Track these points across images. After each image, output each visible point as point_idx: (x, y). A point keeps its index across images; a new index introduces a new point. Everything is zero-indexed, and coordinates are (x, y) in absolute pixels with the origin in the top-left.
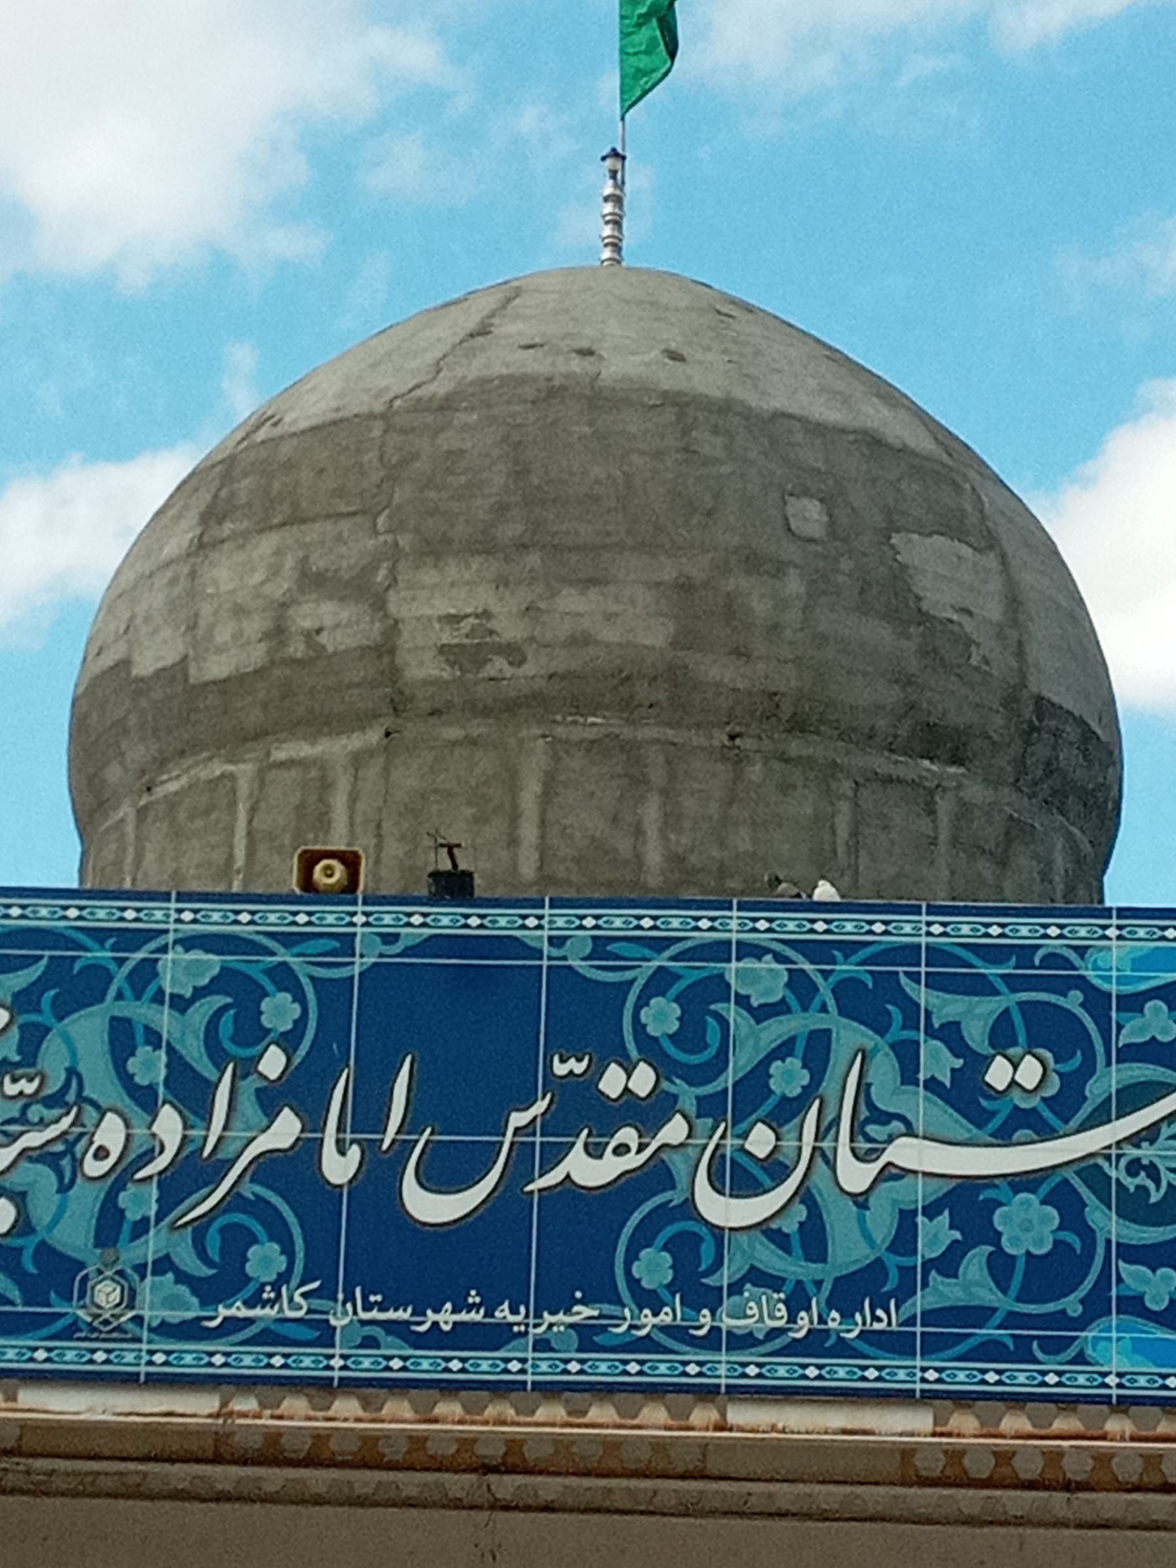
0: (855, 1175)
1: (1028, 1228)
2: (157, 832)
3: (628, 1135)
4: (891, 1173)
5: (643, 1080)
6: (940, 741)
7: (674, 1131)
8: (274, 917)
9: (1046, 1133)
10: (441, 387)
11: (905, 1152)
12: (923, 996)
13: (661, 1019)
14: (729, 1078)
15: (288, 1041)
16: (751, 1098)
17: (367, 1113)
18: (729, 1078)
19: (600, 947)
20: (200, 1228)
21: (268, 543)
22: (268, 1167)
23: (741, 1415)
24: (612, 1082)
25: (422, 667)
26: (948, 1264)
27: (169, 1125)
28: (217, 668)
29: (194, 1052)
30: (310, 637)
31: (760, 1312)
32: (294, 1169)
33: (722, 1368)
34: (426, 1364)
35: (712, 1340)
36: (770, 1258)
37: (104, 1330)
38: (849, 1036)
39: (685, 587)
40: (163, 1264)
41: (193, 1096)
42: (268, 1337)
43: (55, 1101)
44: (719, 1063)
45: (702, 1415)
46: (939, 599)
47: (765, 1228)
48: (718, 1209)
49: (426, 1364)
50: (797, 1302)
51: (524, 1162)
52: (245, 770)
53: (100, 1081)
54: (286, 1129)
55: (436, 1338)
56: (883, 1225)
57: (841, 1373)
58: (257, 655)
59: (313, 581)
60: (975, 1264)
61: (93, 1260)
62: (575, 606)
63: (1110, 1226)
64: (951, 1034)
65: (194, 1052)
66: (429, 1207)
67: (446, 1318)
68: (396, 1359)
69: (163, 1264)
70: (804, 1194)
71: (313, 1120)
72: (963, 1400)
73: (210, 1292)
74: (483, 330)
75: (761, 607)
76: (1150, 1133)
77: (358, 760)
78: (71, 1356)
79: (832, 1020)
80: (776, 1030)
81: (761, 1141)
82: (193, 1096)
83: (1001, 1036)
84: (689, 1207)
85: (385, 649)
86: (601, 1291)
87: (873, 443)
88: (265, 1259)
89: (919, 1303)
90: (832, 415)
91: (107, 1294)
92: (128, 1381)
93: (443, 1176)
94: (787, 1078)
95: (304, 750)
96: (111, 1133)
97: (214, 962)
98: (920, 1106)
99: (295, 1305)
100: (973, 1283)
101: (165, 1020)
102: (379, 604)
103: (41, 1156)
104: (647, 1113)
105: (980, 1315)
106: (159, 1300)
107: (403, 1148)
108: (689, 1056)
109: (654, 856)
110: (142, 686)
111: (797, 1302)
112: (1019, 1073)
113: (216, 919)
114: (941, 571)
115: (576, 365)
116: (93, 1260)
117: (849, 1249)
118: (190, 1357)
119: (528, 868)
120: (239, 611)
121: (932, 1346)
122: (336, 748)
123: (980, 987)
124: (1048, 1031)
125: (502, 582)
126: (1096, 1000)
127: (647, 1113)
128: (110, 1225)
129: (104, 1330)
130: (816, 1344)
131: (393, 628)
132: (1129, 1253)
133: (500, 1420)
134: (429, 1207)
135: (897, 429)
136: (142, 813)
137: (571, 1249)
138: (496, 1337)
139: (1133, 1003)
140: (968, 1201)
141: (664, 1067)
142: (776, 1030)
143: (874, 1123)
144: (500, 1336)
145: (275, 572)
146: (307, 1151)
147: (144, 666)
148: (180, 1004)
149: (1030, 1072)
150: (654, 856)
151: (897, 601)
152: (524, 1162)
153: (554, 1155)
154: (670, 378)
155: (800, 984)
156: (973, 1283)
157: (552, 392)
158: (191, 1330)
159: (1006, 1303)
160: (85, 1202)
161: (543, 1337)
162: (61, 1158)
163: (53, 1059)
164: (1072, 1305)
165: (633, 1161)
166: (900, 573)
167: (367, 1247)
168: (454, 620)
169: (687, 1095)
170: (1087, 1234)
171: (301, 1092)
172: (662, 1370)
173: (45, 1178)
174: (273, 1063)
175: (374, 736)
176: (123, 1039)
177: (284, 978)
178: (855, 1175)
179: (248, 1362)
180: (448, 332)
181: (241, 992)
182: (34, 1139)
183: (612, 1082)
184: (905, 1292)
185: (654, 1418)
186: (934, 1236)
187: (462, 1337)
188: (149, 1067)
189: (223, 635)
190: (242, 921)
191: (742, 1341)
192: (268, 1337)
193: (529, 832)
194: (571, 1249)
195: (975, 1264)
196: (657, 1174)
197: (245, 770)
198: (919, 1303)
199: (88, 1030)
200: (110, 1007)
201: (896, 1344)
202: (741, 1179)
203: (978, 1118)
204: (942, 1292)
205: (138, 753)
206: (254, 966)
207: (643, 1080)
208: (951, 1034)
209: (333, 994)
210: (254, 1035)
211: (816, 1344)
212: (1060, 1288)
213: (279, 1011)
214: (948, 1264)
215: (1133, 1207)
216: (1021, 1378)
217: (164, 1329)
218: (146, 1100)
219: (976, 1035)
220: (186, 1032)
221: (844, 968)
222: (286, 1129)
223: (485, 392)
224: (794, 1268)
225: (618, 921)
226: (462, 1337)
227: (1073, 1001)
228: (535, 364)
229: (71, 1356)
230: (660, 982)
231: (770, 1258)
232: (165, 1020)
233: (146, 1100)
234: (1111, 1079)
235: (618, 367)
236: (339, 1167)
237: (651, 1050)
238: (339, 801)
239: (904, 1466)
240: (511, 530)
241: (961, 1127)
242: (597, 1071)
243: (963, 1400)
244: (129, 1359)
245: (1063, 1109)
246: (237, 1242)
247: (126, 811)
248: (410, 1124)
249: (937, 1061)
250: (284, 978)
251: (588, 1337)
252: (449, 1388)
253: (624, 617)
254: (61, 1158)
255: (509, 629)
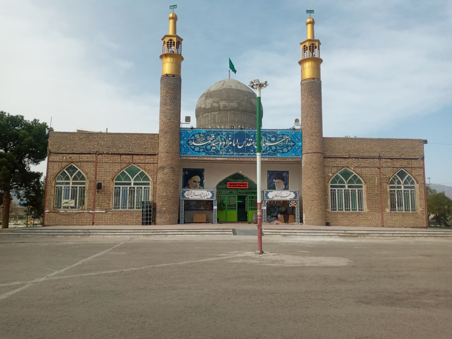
0: (264, 145)
1: (274, 148)
2: (203, 119)
5: (251, 140)
7: (253, 143)
8: (229, 130)
10: (221, 89)
11: (266, 144)
13: (252, 136)
17: (235, 142)
24: (250, 140)
25: (222, 108)
26: (269, 150)
27: (224, 143)
28: (207, 107)
29: (225, 138)
39: (238, 103)
41: (225, 141)
46: (254, 103)
49: (239, 156)
51: (245, 145)
52: (210, 114)
53: (220, 140)
54: (231, 143)
55: (240, 155)
56: (265, 148)
59: (214, 102)
60: (271, 150)
62: (232, 104)
63: (278, 148)
64: (269, 137)
65: (225, 138)
66: (239, 147)
68: (238, 156)
73: (227, 152)
75: (243, 104)
77: (217, 114)
82: (225, 141)
83: (272, 137)
85: (219, 107)
87: (249, 92)
88: (230, 150)
90: (246, 90)
91: (221, 152)
96: (221, 143)
98: (267, 141)
99: (232, 153)
100: (270, 151)
104: (252, 142)
106: (224, 153)
110: (202, 108)
112: (273, 139)
113: (226, 130)
118: (226, 156)
119: (229, 121)
122: (216, 113)
123: (271, 134)
126: (277, 135)
127: (252, 142)
128: (221, 149)
134: (239, 147)
139: (280, 135)
140: (270, 147)
141: (253, 139)
144: (244, 155)
146: (232, 144)
147: (202, 107)
149: (274, 139)
152: (245, 145)
154: (236, 88)
156: (270, 151)
157: (229, 89)
160: (219, 147)
166: (251, 101)
171: (232, 141)
174: (230, 139)
176: (221, 138)
177: (230, 134)
178: (264, 145)
180: (222, 83)
181: (228, 135)
186: (268, 149)
187: (241, 155)
188: (223, 139)
190: (228, 130)
195: (271, 150)
196: (252, 145)
197: (210, 114)
199: (219, 137)
201: (266, 155)
204: (269, 152)
205: (202, 113)
207: (251, 140)
208: (269, 137)
209: (233, 135)
210: (229, 137)
212: (275, 152)
213: (230, 136)
214: (269, 150)
215: (280, 147)
219: (271, 137)
220: (225, 137)
222: (231, 143)
223: (225, 89)
226: (241, 155)
228: (228, 87)
230: (252, 134)
234: (278, 139)
235: (233, 87)
236: (234, 145)
237: (252, 138)
239: (267, 161)
240: (227, 99)
244: (222, 156)
246: (228, 149)
247: (201, 116)
249: (268, 138)
250: (230, 134)
251: (249, 155)
253: (234, 104)
254: (218, 145)
255: (227, 106)
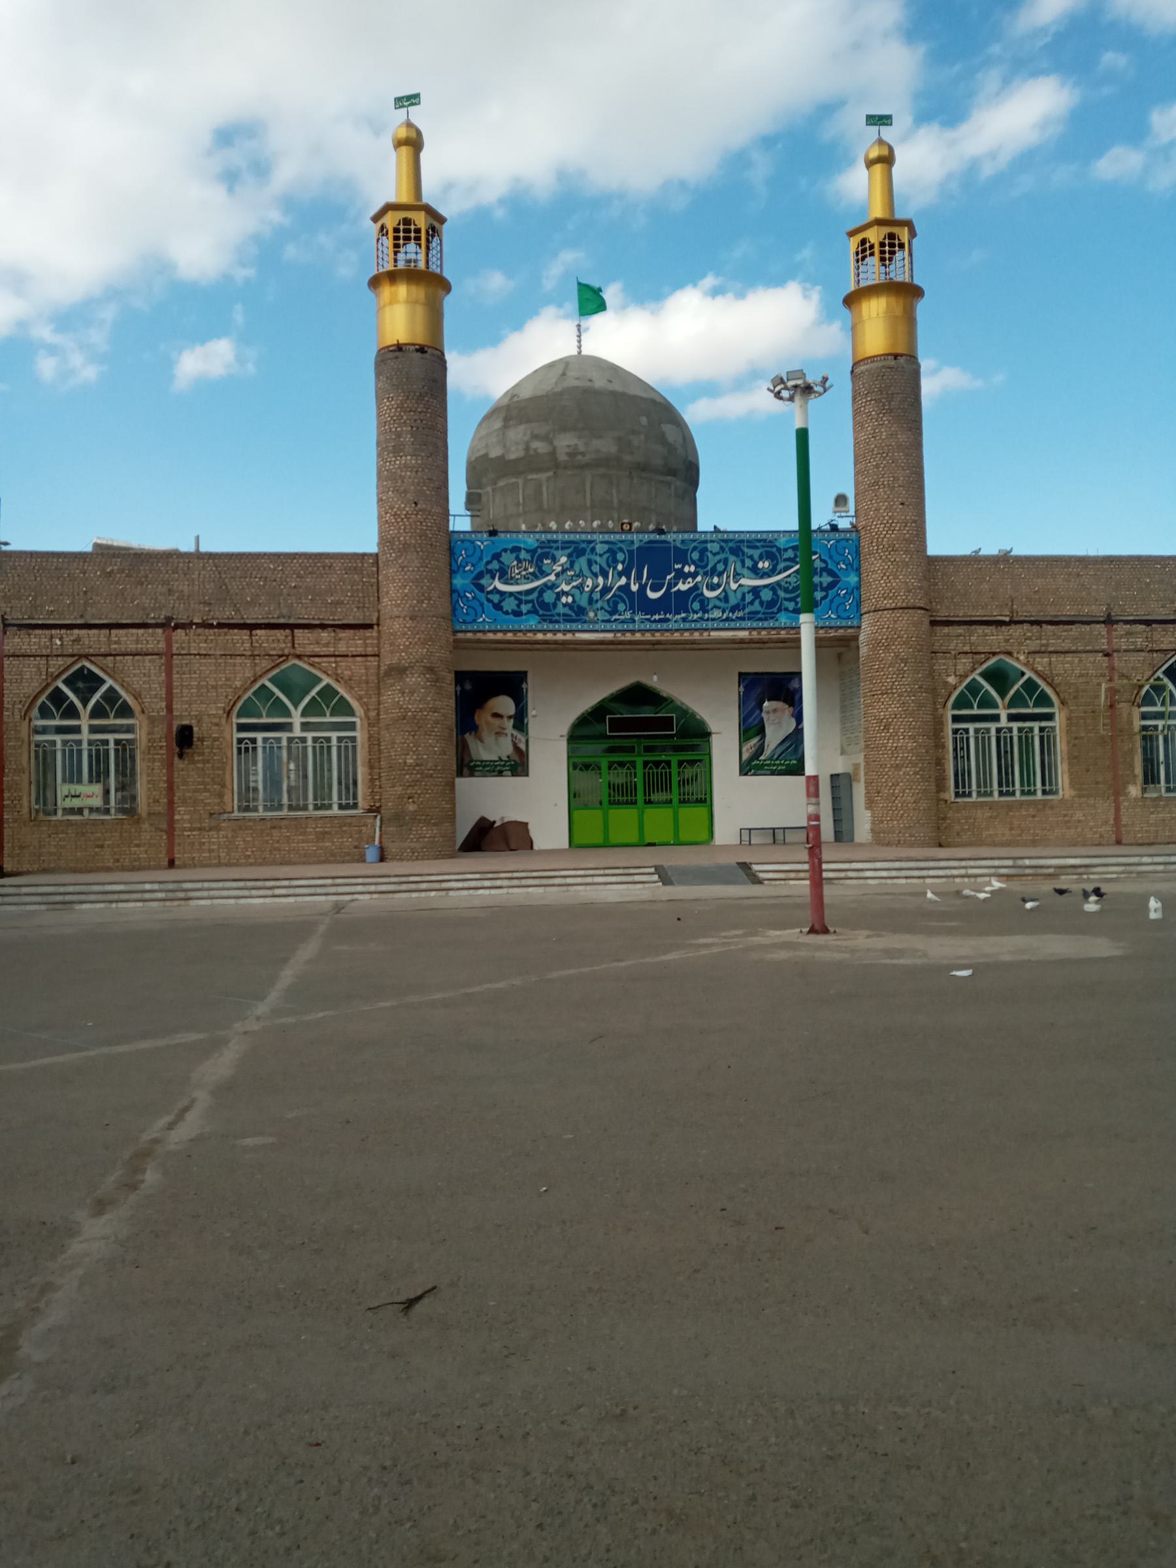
1: (767, 595)
3: (690, 580)
4: (740, 586)
6: (672, 472)
7: (699, 578)
8: (618, 537)
9: (770, 576)
10: (558, 389)
11: (743, 581)
12: (746, 550)
13: (695, 556)
14: (709, 568)
15: (623, 563)
16: (714, 571)
17: (639, 577)
18: (709, 568)
19: (683, 541)
20: (608, 601)
21: (522, 427)
22: (620, 588)
23: (712, 633)
24: (686, 569)
25: (562, 457)
26: (752, 603)
27: (601, 580)
28: (512, 456)
29: (605, 566)
30: (535, 450)
31: (716, 614)
32: (626, 588)
33: (710, 625)
34: (654, 626)
35: (708, 620)
36: (718, 603)
37: (591, 622)
38: (732, 558)
39: (619, 439)
40: (602, 608)
41: (605, 575)
42: (623, 622)
43: (578, 576)
44: (707, 565)
45: (706, 634)
47: (717, 597)
48: (708, 594)
49: (654, 626)
50: (723, 612)
51: (670, 587)
53: (586, 572)
54: (623, 581)
56: (739, 595)
57: (732, 625)
58: (521, 454)
59: (535, 437)
60: (757, 602)
61: (588, 607)
62: (596, 443)
63: (782, 594)
64: (751, 557)
66: (652, 595)
67: (657, 617)
69: (602, 608)
70: (724, 590)
71: (629, 578)
72: (754, 629)
73: (611, 613)
74: (564, 374)
76: (789, 576)
77: (548, 479)
78: (586, 627)
79: (728, 555)
80: (718, 557)
81: (716, 580)
82: (605, 575)
83: (761, 558)
84: (702, 594)
86: (687, 611)
88: (621, 607)
89: (747, 611)
91: (591, 614)
92: (597, 631)
93: (655, 589)
94: (720, 567)
95: (535, 476)
96: (589, 582)
97: (606, 547)
98: (745, 572)
99: (628, 615)
100: (756, 606)
101: (598, 559)
102: (551, 443)
103: (576, 587)
104: (694, 575)
105: (758, 613)
106: (602, 615)
107: (646, 584)
108: (701, 564)
109: (615, 501)
111: (723, 612)
112: (764, 565)
114: (669, 430)
115: (589, 384)
116: (588, 607)
117: (733, 601)
118: (608, 626)
120: (517, 443)
121: (749, 619)
122: (543, 476)
124: (770, 556)
125: (579, 437)
126: (779, 550)
128: (591, 601)
129: (591, 622)
130: (727, 619)
131: (555, 449)
132: (786, 599)
133: (667, 636)
135: (658, 400)
136: (494, 490)
137: (681, 602)
138: (667, 620)
139: (786, 550)
140: (755, 591)
142: (718, 557)
143: (737, 576)
144: (667, 620)
145: (525, 434)
146: (628, 585)
148: (601, 555)
149: (767, 564)
150: (615, 501)
151: (662, 439)
152: (670, 587)
153: (676, 584)
154: (611, 387)
155: (722, 549)
156: (756, 606)
158: (608, 621)
159: (553, 551)
160: (585, 597)
161: (676, 620)
162: (580, 587)
163: (577, 567)
164: (775, 610)
165: (691, 585)
167: (641, 603)
168: (569, 446)
169: (701, 571)
170: (778, 596)
171: (626, 573)
172: (698, 626)
173: (577, 592)
174: (620, 567)
175: (551, 474)
176: (590, 563)
177: (621, 549)
178: (734, 586)
179: (620, 627)
181: (612, 552)
182: (574, 584)
183: (686, 569)
184: (744, 609)
185: (696, 635)
187: (660, 621)
188: (596, 568)
189: (513, 449)
190: (612, 537)
191: (713, 620)
192: (623, 622)
193: (588, 495)
194: (681, 602)
195: (757, 602)
197: (520, 481)
198: (747, 611)
200: (587, 556)
201: (742, 619)
202: (712, 588)
203: (757, 574)
206: (615, 547)
207: (693, 568)
208: (751, 557)
209: (631, 552)
210: (616, 561)
211: (727, 619)
213: (620, 556)
214: (752, 603)
215: (786, 590)
216: (766, 624)
217: (603, 621)
218: (595, 575)
219: (756, 557)
220: (602, 561)
221: (731, 544)
222: (623, 581)
224: (722, 605)
225: (686, 536)
226: (660, 621)
227: (774, 550)
229: (586, 627)
230: (695, 549)
231: (718, 603)
232: (598, 559)
233: (595, 575)
234: (781, 565)
237: (694, 562)
238: (544, 489)
241: (752, 575)
242: (683, 567)
243: (754, 629)
244: (597, 627)
245: (772, 572)
246: (616, 604)
248: (648, 579)
249: (749, 563)
250: (621, 549)
251: (684, 620)
252: (657, 631)
253: (606, 446)
254: (580, 587)
255: (582, 448)
